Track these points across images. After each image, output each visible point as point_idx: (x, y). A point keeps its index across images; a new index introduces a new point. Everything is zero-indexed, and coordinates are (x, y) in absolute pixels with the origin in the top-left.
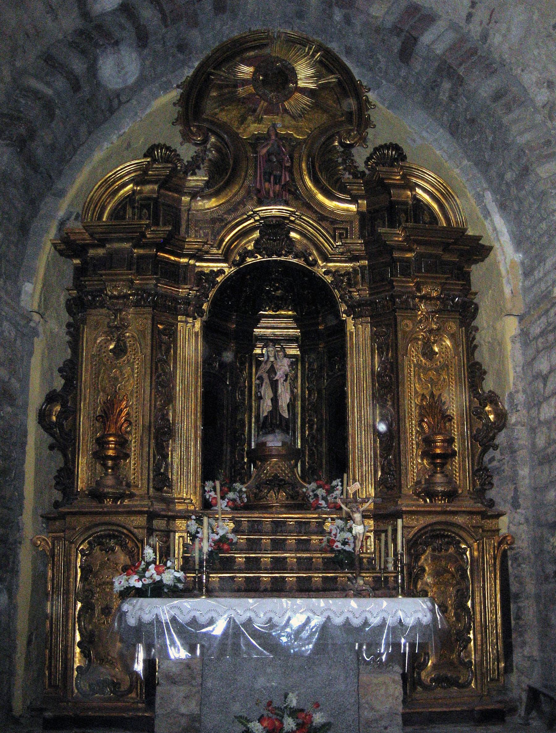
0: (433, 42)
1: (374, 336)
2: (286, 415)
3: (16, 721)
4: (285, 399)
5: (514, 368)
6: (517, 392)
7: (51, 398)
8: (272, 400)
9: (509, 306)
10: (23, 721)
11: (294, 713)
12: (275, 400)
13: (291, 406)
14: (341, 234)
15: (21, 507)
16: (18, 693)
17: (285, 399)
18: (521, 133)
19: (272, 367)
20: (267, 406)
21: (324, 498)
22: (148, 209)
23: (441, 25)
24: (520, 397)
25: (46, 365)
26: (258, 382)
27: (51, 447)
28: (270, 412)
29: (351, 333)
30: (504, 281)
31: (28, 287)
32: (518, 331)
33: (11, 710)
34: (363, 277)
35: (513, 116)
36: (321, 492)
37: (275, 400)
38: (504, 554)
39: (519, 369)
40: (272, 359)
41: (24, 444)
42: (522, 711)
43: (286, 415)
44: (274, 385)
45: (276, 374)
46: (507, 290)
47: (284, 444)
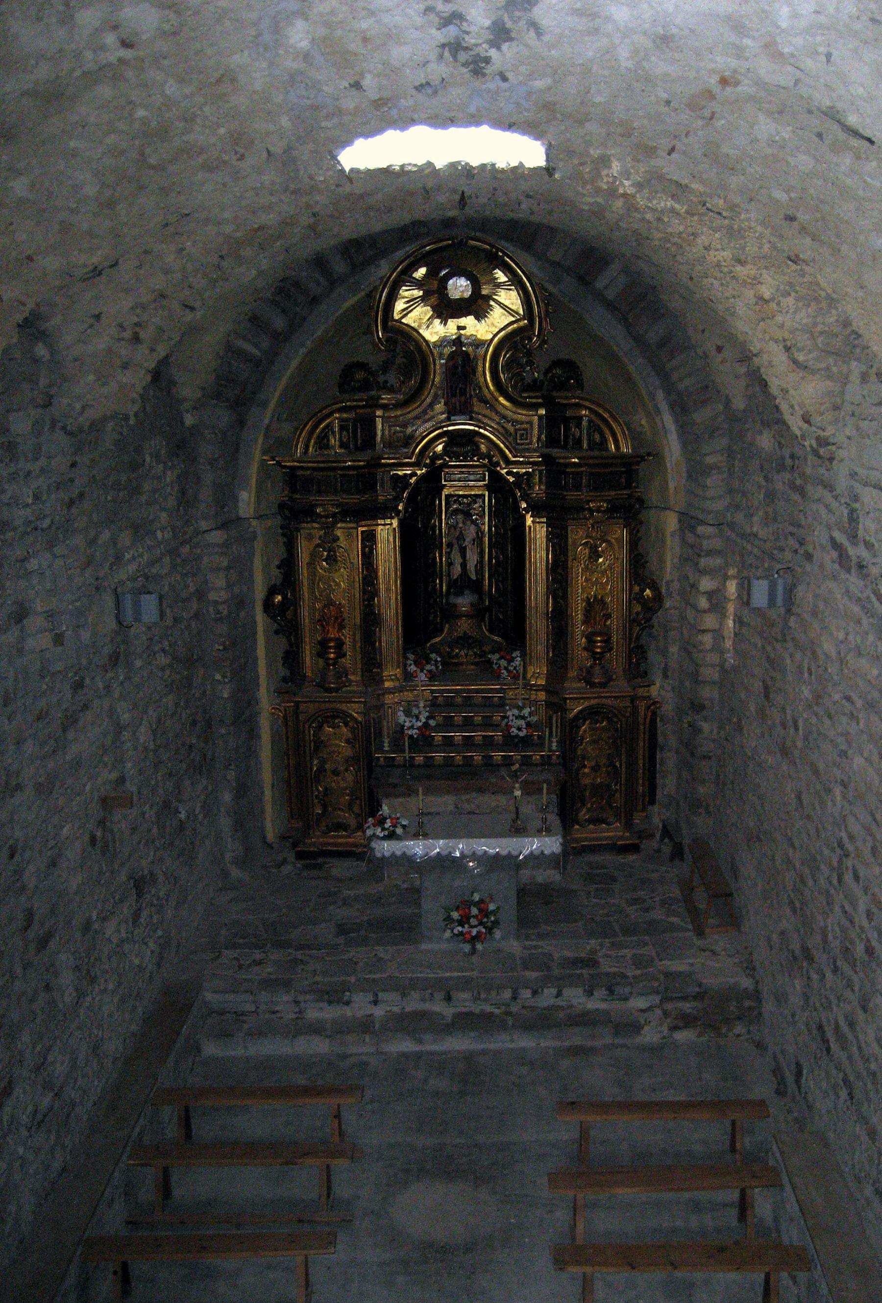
0: (606, 288)
1: (548, 533)
2: (473, 577)
3: (270, 846)
4: (472, 559)
5: (672, 560)
6: (672, 581)
7: (272, 591)
8: (461, 565)
9: (672, 502)
10: (274, 845)
11: (476, 904)
12: (464, 565)
13: (479, 570)
14: (522, 435)
15: (258, 685)
16: (268, 825)
17: (472, 559)
18: (681, 380)
19: (461, 533)
20: (457, 570)
21: (506, 668)
22: (348, 431)
23: (614, 269)
24: (676, 585)
25: (265, 560)
26: (448, 550)
27: (277, 632)
28: (461, 575)
29: (530, 527)
30: (670, 476)
31: (244, 495)
32: (677, 527)
33: (264, 837)
34: (540, 479)
35: (675, 362)
36: (503, 663)
37: (464, 565)
38: (654, 714)
39: (676, 560)
40: (461, 525)
41: (255, 633)
42: (658, 836)
43: (473, 577)
44: (463, 551)
45: (464, 540)
46: (671, 485)
47: (472, 605)
